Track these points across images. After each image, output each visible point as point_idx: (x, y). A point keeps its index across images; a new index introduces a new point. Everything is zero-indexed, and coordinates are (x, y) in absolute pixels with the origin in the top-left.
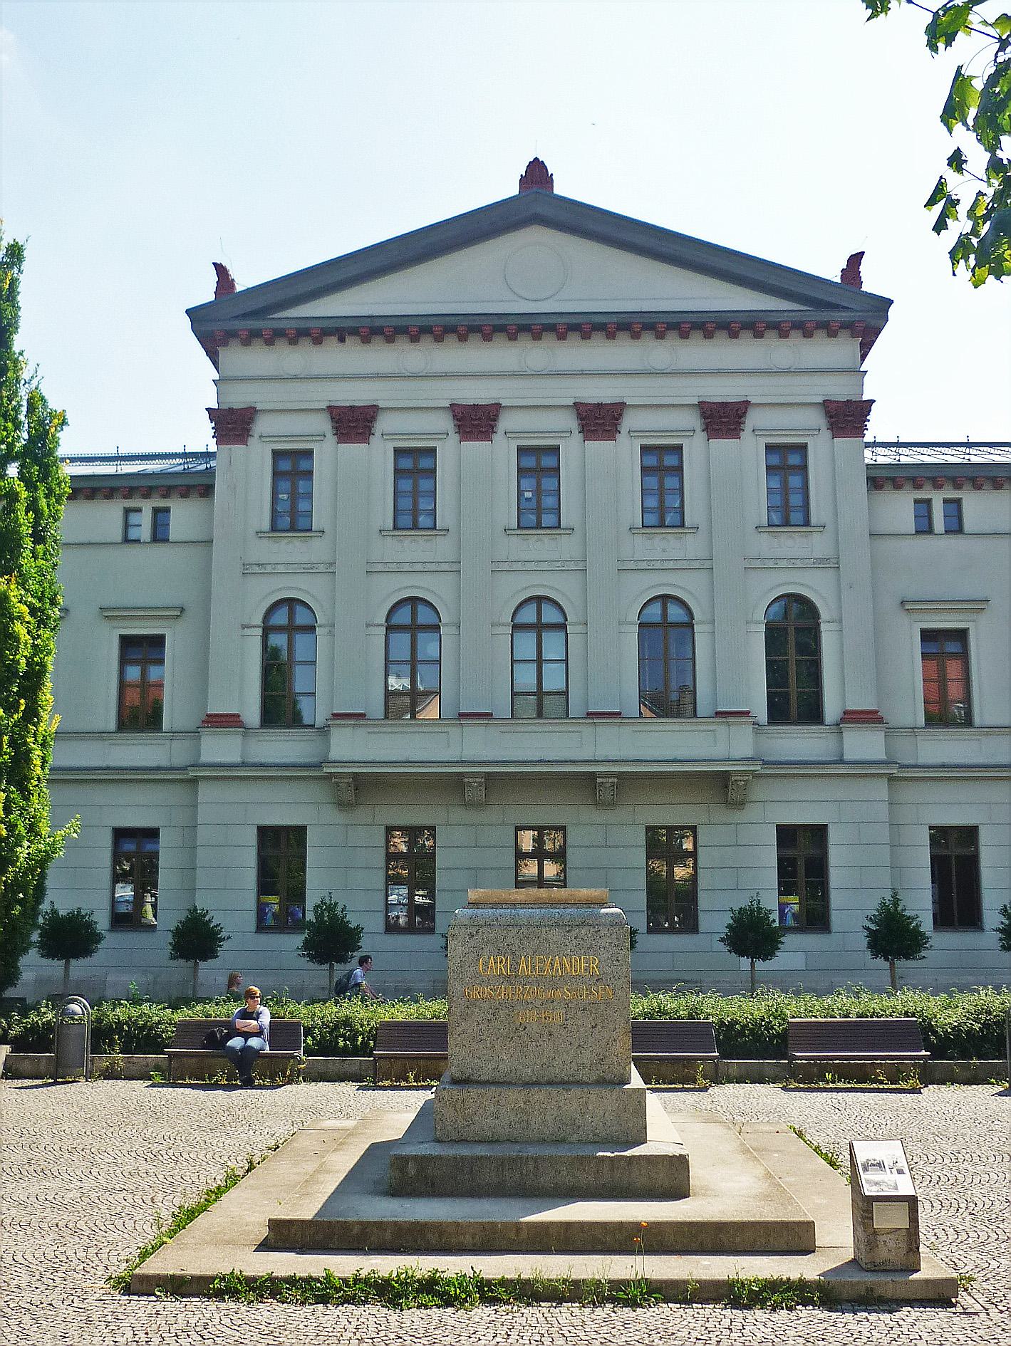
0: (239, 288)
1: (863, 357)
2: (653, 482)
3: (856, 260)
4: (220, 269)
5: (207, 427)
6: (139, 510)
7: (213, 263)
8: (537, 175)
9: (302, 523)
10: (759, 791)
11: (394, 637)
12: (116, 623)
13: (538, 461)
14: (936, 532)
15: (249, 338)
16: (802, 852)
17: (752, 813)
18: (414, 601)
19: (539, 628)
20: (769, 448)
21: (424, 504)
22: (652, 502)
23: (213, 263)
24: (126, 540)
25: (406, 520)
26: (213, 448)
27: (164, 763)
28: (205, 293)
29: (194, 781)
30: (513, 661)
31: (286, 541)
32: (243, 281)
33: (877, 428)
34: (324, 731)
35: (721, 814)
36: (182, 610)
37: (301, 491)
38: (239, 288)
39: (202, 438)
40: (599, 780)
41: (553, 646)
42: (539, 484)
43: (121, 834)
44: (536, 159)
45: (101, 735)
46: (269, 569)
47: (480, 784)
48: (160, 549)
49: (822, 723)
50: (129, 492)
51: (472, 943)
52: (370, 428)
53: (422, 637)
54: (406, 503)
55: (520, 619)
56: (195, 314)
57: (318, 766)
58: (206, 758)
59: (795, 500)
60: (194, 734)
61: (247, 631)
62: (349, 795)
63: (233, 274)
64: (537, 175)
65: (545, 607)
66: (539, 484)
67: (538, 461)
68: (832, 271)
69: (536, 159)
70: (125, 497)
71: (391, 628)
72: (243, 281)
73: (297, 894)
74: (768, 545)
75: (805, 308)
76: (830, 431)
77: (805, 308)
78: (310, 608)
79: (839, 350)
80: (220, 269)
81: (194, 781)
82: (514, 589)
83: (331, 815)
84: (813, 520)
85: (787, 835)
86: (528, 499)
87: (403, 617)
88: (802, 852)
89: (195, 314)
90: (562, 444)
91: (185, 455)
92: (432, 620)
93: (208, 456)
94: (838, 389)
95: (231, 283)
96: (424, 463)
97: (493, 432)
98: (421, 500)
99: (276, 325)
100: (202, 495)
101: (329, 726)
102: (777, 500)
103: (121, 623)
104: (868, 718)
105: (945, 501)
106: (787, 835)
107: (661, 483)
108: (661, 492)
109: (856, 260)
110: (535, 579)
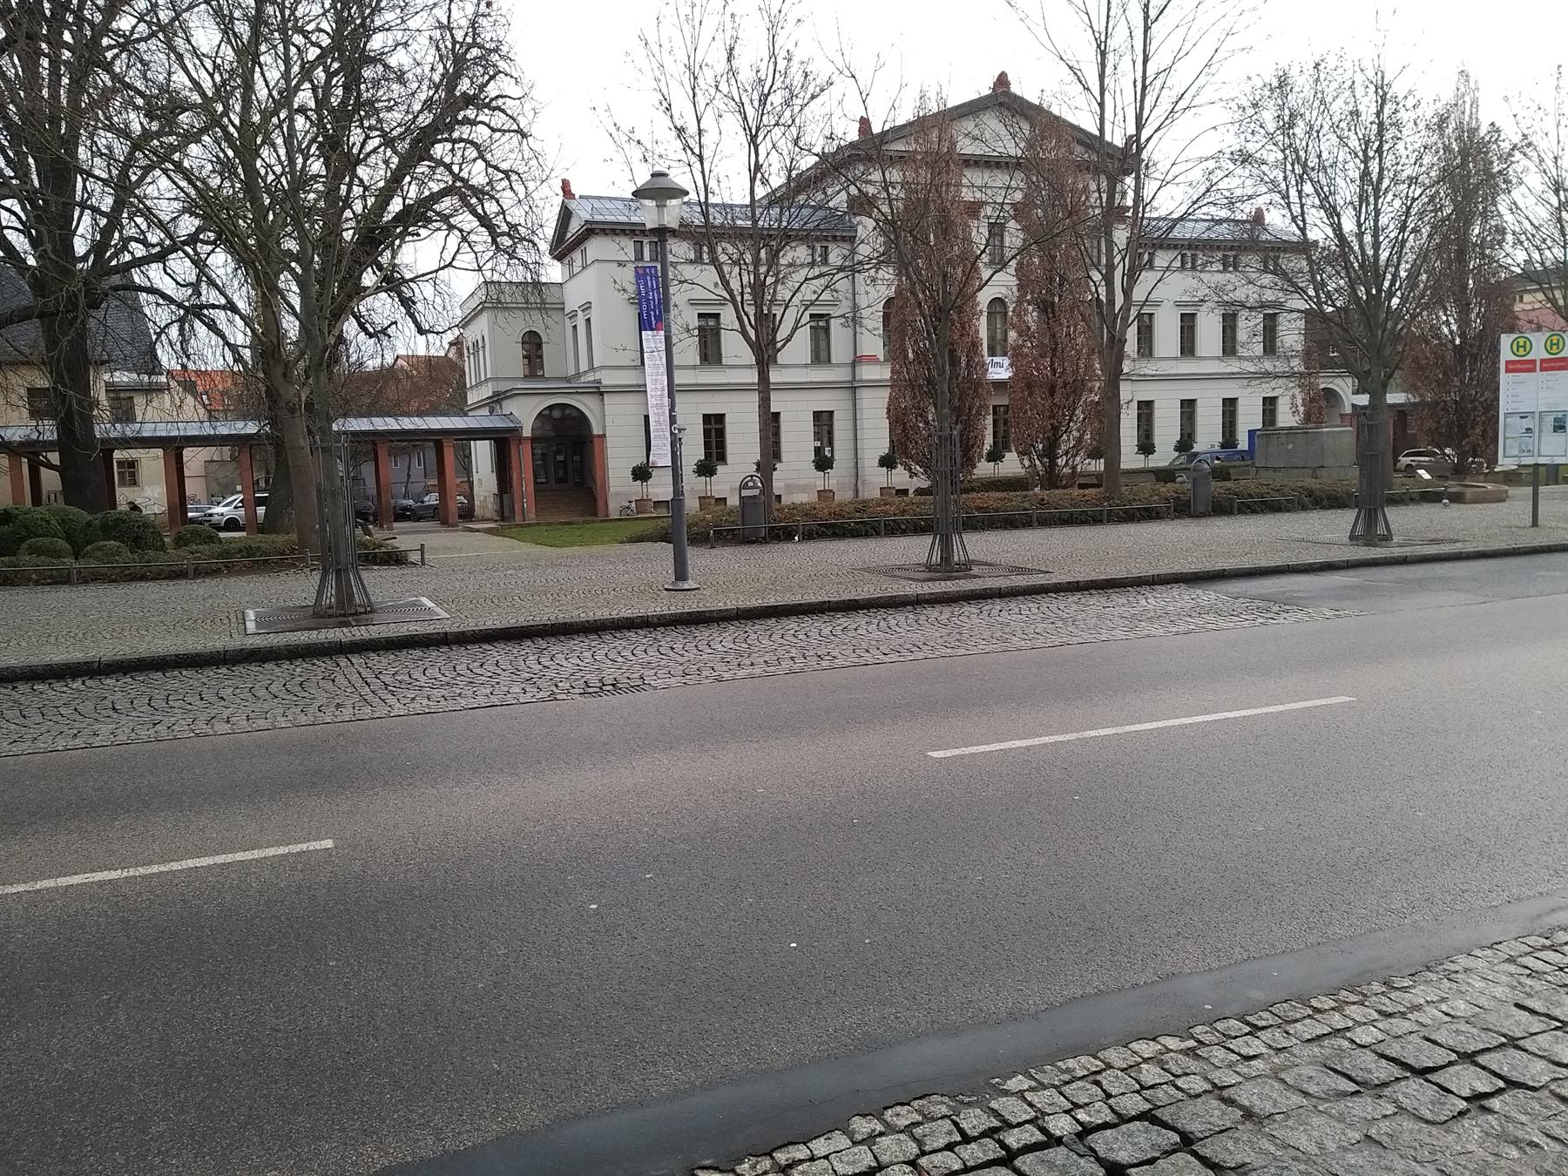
8: (1002, 80)
64: (1002, 80)
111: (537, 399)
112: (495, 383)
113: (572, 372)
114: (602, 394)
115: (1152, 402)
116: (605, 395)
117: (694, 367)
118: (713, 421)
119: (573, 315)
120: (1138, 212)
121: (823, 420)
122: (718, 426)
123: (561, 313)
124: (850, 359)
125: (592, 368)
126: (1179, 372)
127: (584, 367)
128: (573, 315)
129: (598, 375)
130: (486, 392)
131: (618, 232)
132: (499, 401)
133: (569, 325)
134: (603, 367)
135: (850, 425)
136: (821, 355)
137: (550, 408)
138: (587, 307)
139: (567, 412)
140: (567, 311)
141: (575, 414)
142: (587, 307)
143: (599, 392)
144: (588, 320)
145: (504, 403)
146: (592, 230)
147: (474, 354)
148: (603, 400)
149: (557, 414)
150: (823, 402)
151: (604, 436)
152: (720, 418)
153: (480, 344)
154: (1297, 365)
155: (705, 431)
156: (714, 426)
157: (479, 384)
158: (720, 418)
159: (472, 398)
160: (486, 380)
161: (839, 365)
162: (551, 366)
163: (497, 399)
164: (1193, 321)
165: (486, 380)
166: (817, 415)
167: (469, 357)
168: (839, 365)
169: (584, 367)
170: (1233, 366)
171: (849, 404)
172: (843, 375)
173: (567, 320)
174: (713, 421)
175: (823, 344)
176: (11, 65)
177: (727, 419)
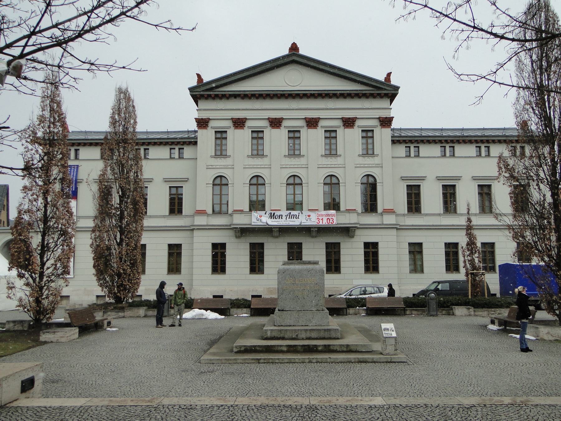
0: (204, 81)
1: (391, 104)
2: (328, 141)
3: (389, 75)
4: (199, 76)
5: (195, 124)
6: (174, 149)
7: (197, 74)
8: (294, 48)
9: (224, 153)
10: (358, 232)
11: (215, 187)
12: (477, 181)
13: (330, 135)
14: (71, 159)
15: (208, 97)
16: (257, 251)
17: (356, 239)
18: (221, 177)
19: (294, 184)
20: (362, 131)
21: (260, 148)
22: (328, 147)
23: (197, 74)
24: (171, 158)
25: (219, 153)
26: (196, 129)
27: (183, 225)
28: (194, 83)
29: (193, 230)
30: (287, 194)
31: (219, 158)
32: (206, 79)
33: (394, 125)
34: (231, 215)
35: (347, 239)
36: (188, 179)
37: (223, 143)
38: (204, 81)
39: (193, 126)
40: (312, 229)
41: (298, 190)
42: (294, 142)
43: (170, 246)
44: (294, 43)
45: (164, 217)
46: (214, 167)
47: (277, 230)
48: (181, 161)
49: (377, 212)
50: (173, 143)
51: (284, 274)
52: (317, 124)
53: (223, 187)
54: (218, 148)
55: (252, 182)
56: (191, 90)
57: (230, 225)
58: (196, 223)
59: (370, 146)
60: (193, 216)
61: (208, 185)
62: (239, 234)
63: (203, 77)
64: (294, 48)
65: (296, 178)
66: (294, 142)
67: (330, 135)
68: (381, 77)
69: (294, 43)
70: (170, 145)
71: (214, 185)
72: (206, 79)
73: (493, 260)
74: (362, 161)
75: (374, 89)
76: (343, 127)
77: (374, 89)
78: (226, 178)
79: (384, 103)
80: (199, 76)
81: (193, 230)
82: (214, 173)
83: (234, 239)
84: (375, 154)
85: (367, 245)
86: (291, 146)
87: (254, 181)
88: (371, 250)
89: (191, 90)
90: (264, 130)
91: (188, 132)
92: (336, 181)
93: (195, 132)
94: (384, 114)
95: (202, 80)
96: (260, 135)
97: (208, 127)
98: (259, 146)
99: (215, 93)
100: (193, 144)
101: (233, 213)
102: (365, 146)
103: (479, 181)
104: (390, 211)
105: (450, 147)
106: (367, 245)
107: (258, 142)
108: (330, 144)
109: (389, 75)
110: (366, 170)
115: (493, 244)
117: (439, 215)
118: (371, 247)
120: (553, 130)
122: (373, 250)
126: (442, 224)
131: (431, 141)
152: (375, 245)
154: (509, 220)
155: (365, 253)
156: (371, 250)
158: (375, 245)
166: (447, 245)
170: (176, 221)
174: (371, 247)
175: (487, 203)
176: (554, 82)
177: (380, 245)
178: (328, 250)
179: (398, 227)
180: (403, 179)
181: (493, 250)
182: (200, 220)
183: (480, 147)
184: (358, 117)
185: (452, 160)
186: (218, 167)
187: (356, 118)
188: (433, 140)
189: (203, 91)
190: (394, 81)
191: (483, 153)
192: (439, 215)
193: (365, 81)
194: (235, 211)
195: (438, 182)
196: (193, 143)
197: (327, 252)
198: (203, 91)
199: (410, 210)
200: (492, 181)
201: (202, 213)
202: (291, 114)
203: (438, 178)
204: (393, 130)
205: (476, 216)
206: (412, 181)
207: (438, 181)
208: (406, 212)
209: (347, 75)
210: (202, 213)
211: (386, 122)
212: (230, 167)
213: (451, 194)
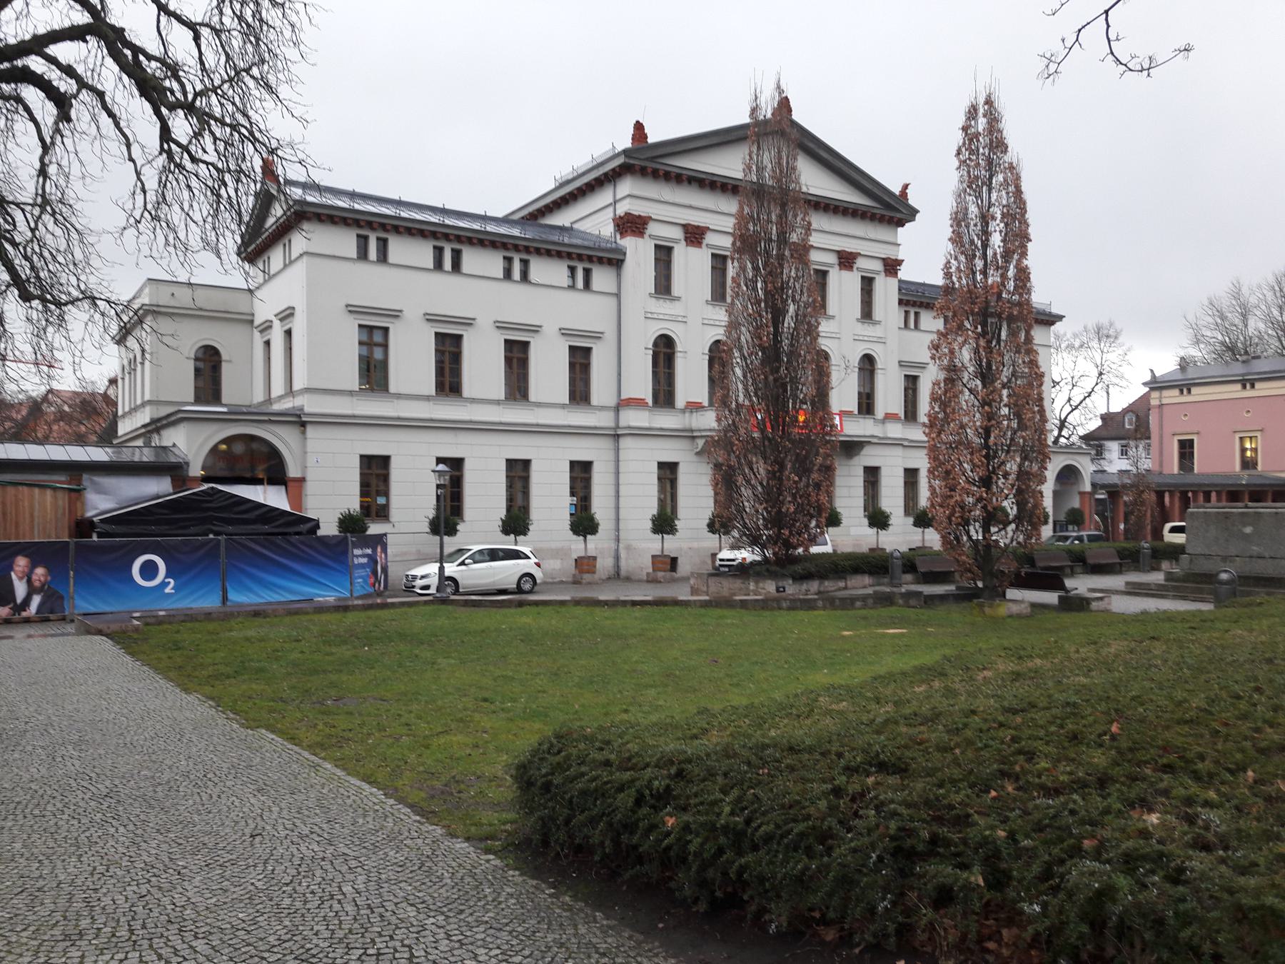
33: (905, 273)
43: (573, 464)
46: (655, 316)
111: (213, 427)
112: (155, 407)
113: (259, 397)
114: (303, 425)
116: (310, 430)
119: (266, 327)
121: (581, 472)
123: (246, 328)
124: (612, 402)
125: (290, 392)
127: (278, 388)
128: (266, 327)
129: (298, 402)
130: (144, 417)
132: (158, 430)
133: (258, 340)
134: (307, 390)
135: (610, 479)
136: (580, 393)
137: (227, 441)
138: (287, 315)
139: (255, 446)
140: (257, 323)
141: (264, 449)
142: (287, 315)
143: (299, 421)
144: (289, 333)
145: (165, 433)
146: (301, 215)
147: (130, 373)
148: (304, 433)
149: (239, 448)
150: (582, 450)
151: (302, 480)
153: (139, 359)
157: (134, 410)
158: (385, 461)
159: (124, 428)
160: (144, 404)
161: (602, 408)
162: (232, 391)
163: (156, 426)
164: (581, 400)
165: (144, 404)
166: (511, 463)
167: (142, 364)
168: (602, 408)
169: (278, 388)
171: (610, 455)
172: (603, 420)
173: (257, 334)
178: (575, 475)
179: (906, 443)
180: (353, 310)
181: (586, 475)
182: (633, 418)
183: (366, 238)
184: (711, 227)
185: (381, 270)
186: (661, 317)
187: (708, 228)
188: (431, 231)
189: (647, 159)
190: (913, 200)
191: (373, 253)
192: (498, 402)
193: (876, 190)
194: (689, 404)
195: (563, 339)
196: (615, 261)
197: (571, 477)
198: (647, 159)
199: (440, 387)
200: (532, 334)
201: (638, 403)
202: (827, 242)
203: (350, 309)
204: (900, 281)
205: (352, 395)
206: (582, 340)
207: (562, 337)
208: (433, 392)
209: (845, 168)
210: (638, 403)
211: (892, 266)
212: (680, 319)
213: (519, 359)
